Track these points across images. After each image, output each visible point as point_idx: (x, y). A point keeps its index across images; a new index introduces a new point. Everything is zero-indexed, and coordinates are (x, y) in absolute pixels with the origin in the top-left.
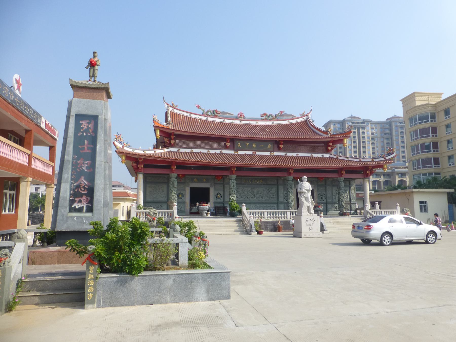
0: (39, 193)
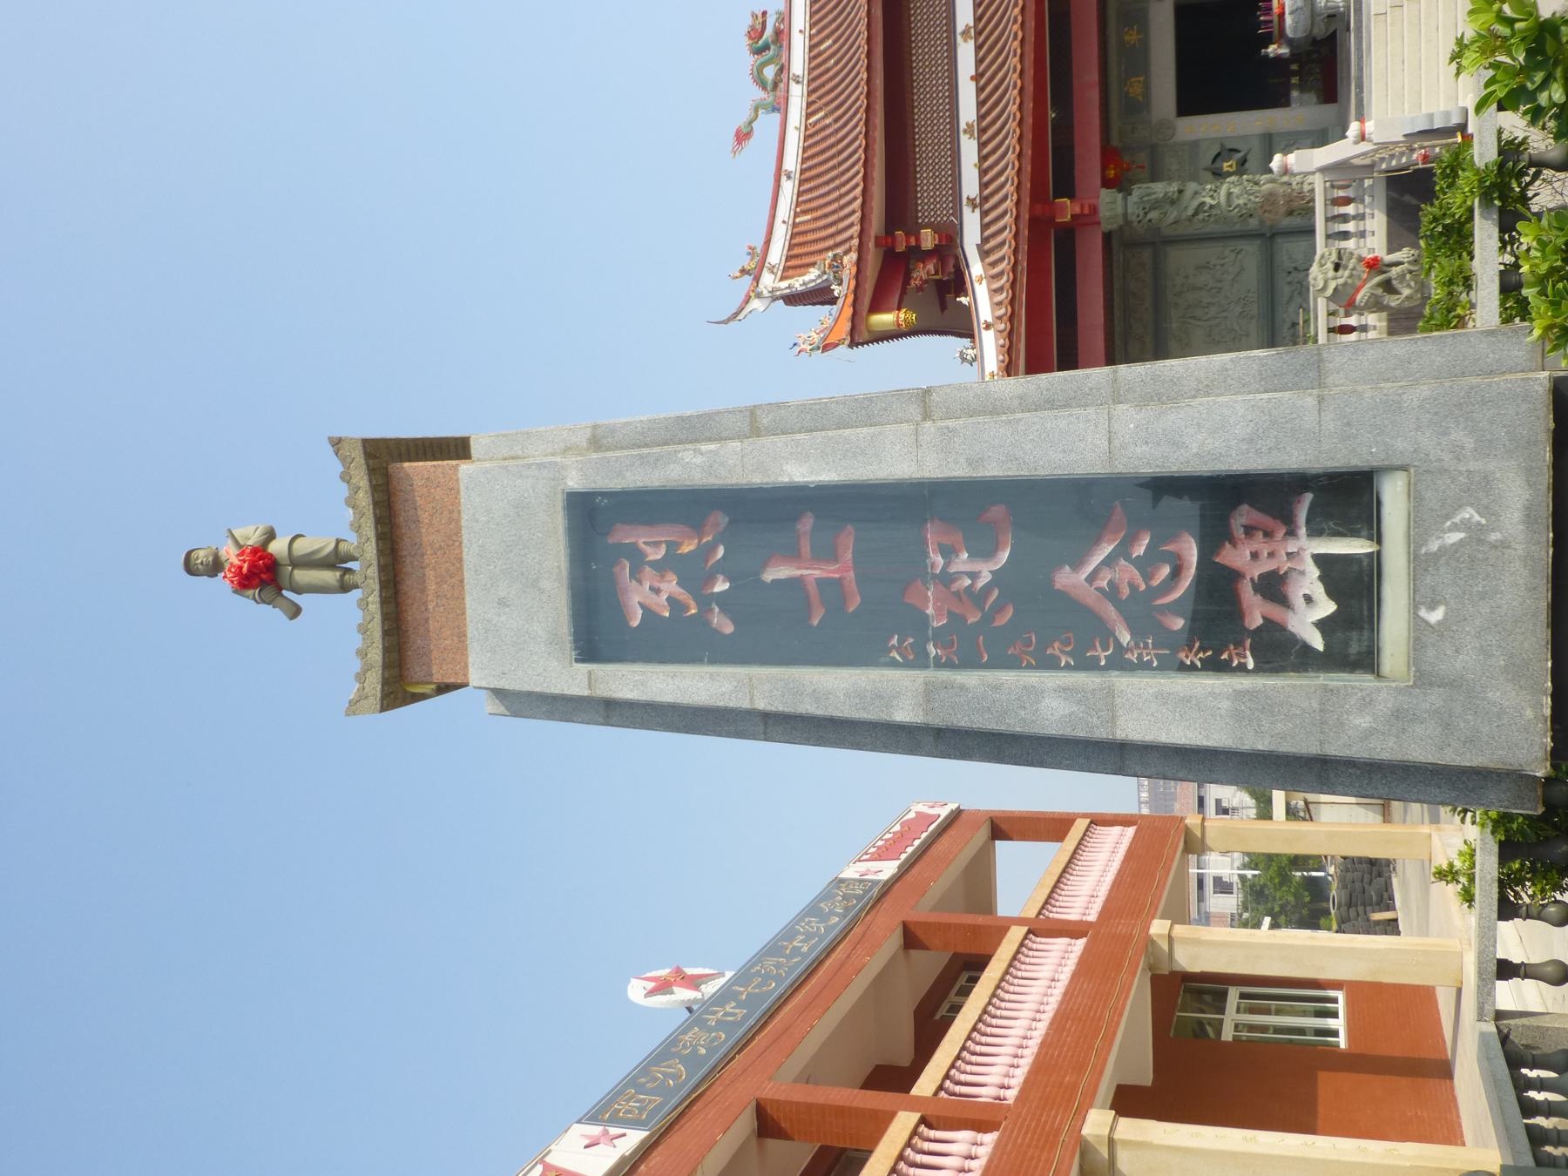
0: (1242, 878)
